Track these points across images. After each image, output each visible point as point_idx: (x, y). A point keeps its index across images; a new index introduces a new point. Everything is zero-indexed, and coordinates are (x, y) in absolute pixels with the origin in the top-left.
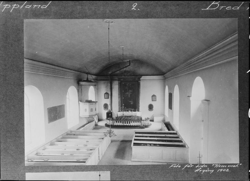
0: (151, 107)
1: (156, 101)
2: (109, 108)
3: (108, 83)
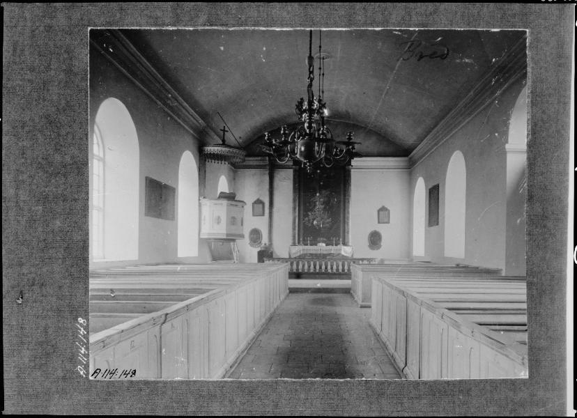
0: (375, 240)
1: (388, 222)
2: (265, 240)
3: (265, 174)
